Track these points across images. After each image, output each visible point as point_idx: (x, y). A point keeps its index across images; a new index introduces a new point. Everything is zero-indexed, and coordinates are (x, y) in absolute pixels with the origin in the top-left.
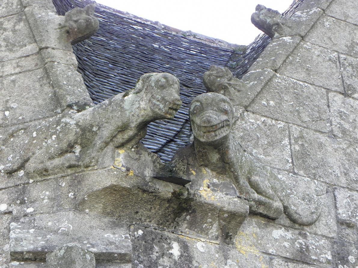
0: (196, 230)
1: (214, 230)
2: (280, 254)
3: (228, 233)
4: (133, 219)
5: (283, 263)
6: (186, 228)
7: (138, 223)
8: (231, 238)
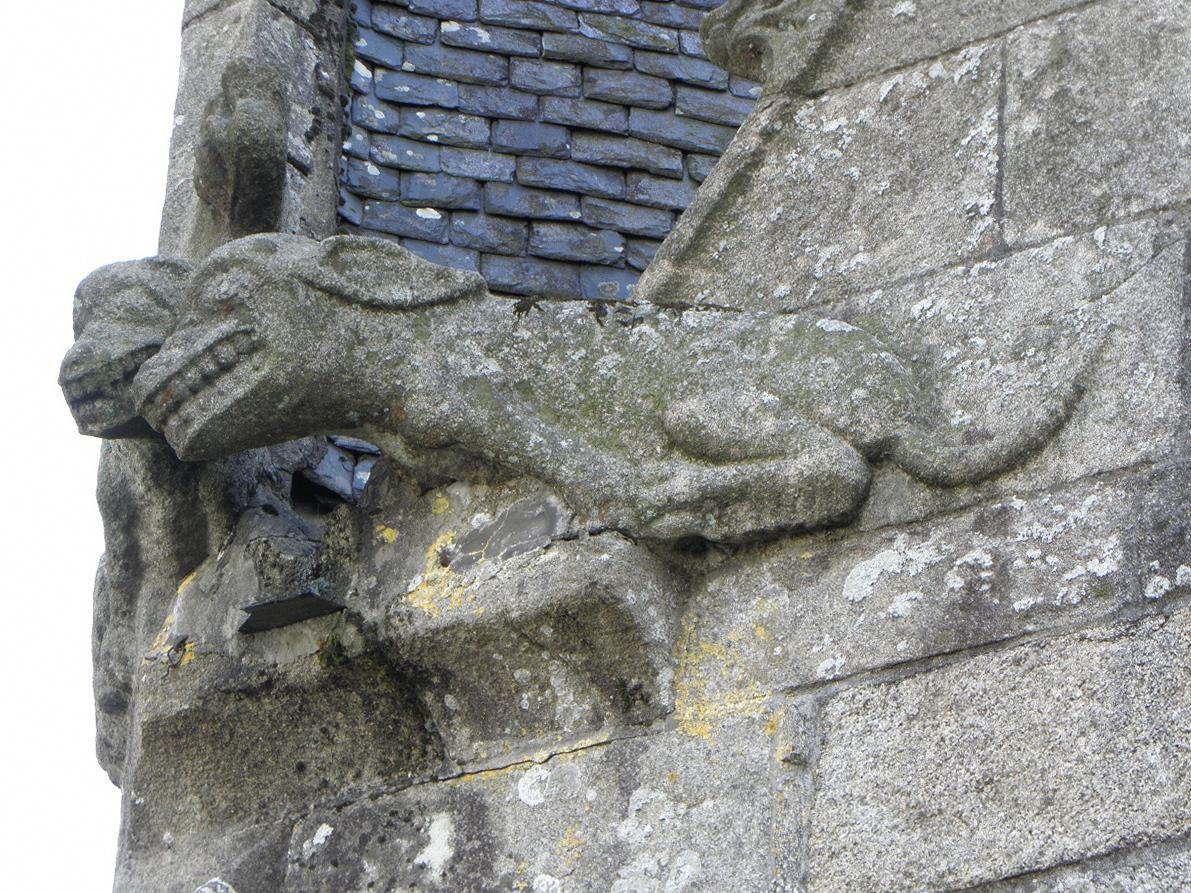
0: (508, 731)
1: (570, 701)
2: (868, 661)
3: (623, 684)
4: (304, 795)
5: (878, 695)
6: (472, 739)
7: (323, 800)
8: (646, 699)
